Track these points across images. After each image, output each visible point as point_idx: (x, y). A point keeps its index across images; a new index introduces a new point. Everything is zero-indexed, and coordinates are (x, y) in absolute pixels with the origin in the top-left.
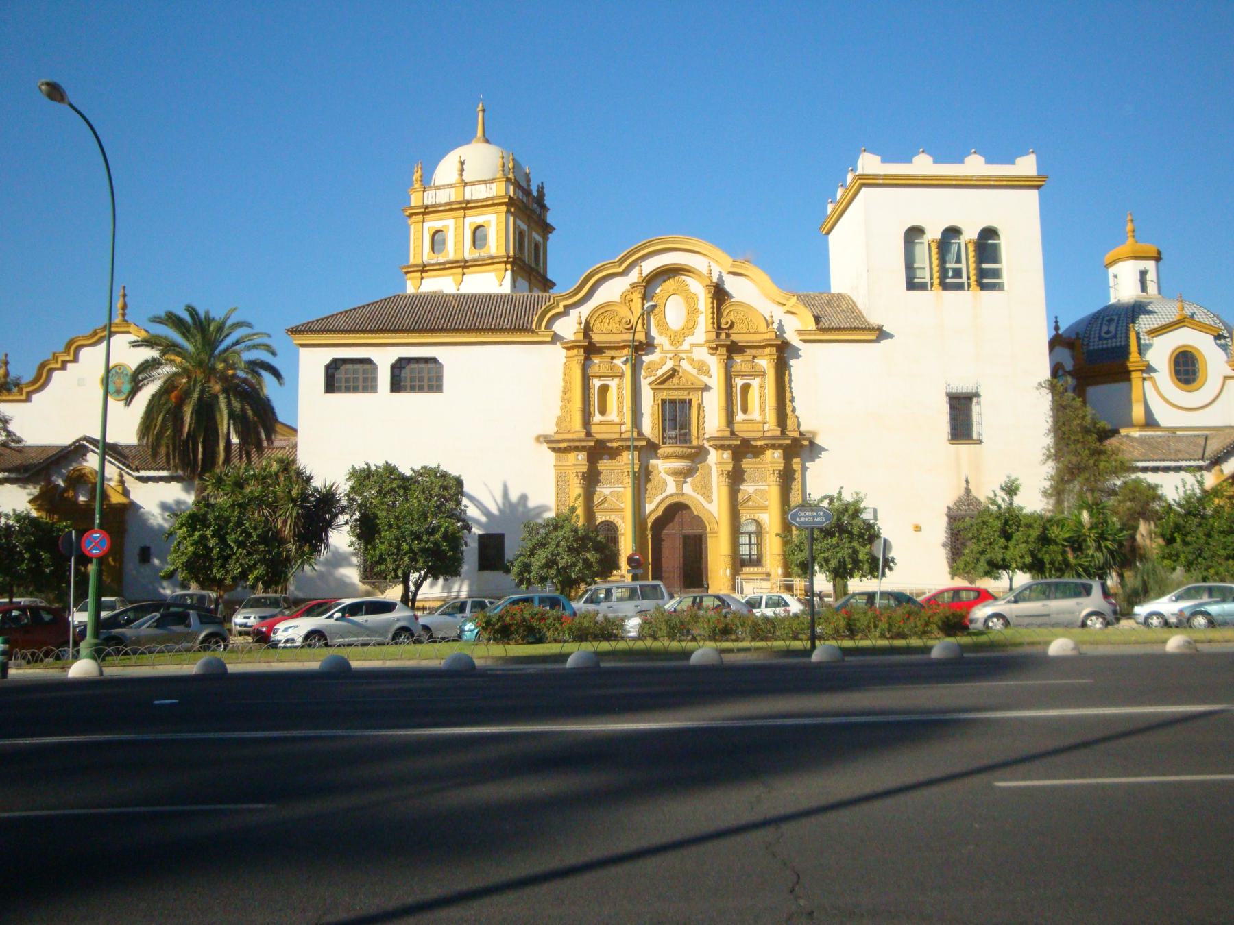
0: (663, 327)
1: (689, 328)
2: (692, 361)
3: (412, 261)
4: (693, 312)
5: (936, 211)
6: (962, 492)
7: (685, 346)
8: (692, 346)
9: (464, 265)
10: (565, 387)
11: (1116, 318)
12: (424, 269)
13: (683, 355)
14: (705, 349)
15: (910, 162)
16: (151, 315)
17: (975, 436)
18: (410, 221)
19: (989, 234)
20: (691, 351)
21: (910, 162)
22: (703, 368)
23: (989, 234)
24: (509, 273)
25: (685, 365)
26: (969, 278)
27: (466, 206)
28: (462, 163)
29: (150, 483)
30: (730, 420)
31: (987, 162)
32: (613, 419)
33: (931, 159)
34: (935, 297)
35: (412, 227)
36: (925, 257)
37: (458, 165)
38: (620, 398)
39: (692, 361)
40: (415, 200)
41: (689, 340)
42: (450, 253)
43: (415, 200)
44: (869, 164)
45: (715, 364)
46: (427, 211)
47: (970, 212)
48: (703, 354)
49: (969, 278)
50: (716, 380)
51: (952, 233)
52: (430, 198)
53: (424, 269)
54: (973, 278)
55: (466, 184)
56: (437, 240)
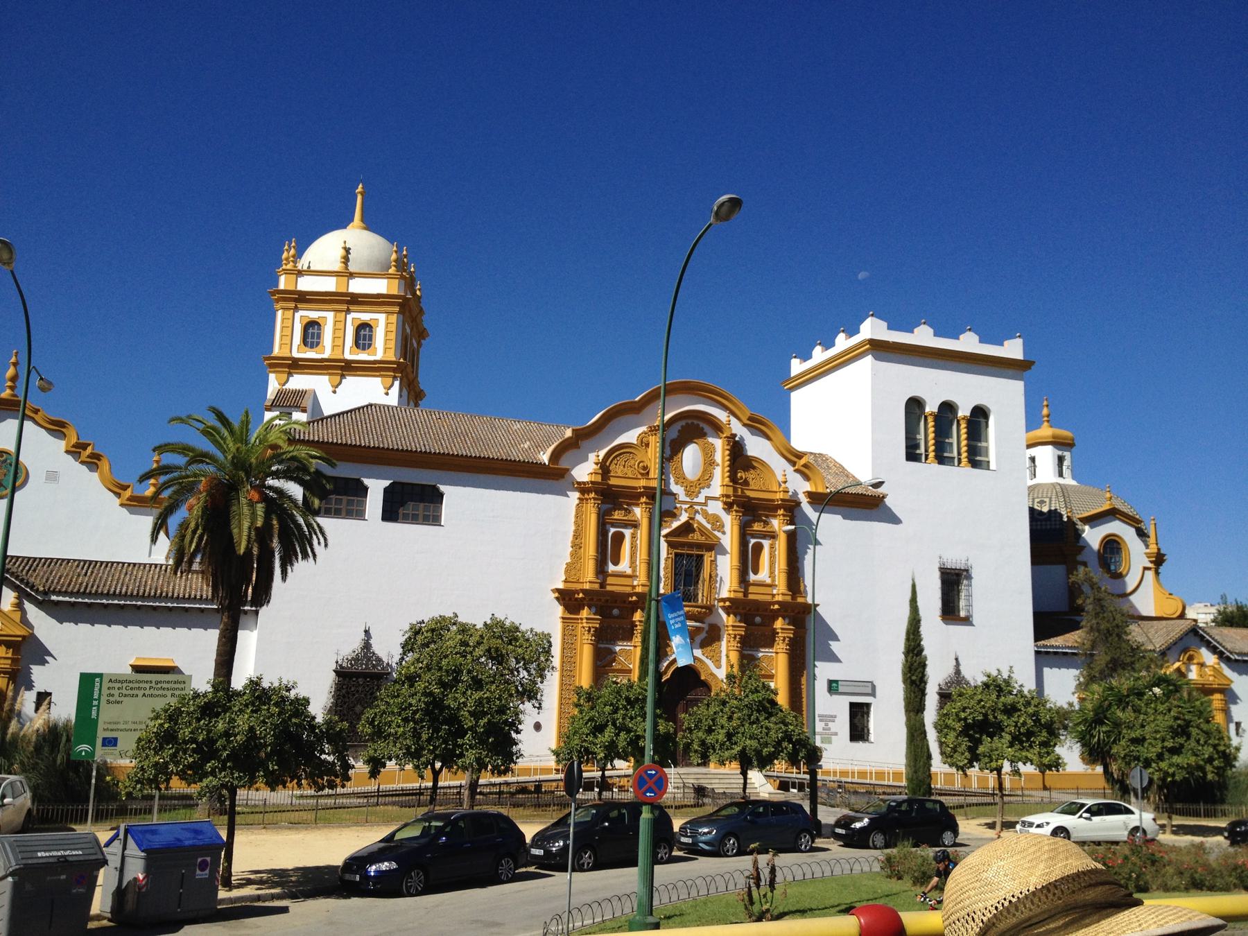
0: (681, 479)
1: (705, 480)
2: (706, 515)
3: (276, 351)
4: (710, 463)
5: (938, 386)
6: (951, 671)
7: (701, 499)
8: (707, 498)
9: (343, 368)
10: (575, 531)
11: (1047, 500)
12: (295, 366)
13: (698, 508)
14: (720, 505)
15: (912, 332)
16: (214, 405)
17: (963, 614)
18: (278, 306)
19: (912, 455)
20: (705, 504)
21: (912, 332)
22: (716, 522)
23: (980, 414)
24: (397, 383)
25: (699, 517)
26: (959, 454)
27: (356, 301)
28: (347, 250)
29: (919, 604)
30: (601, 570)
31: (981, 341)
32: (630, 567)
33: (976, 338)
34: (930, 469)
35: (280, 313)
36: (927, 435)
37: (342, 252)
38: (772, 556)
39: (706, 515)
40: (283, 283)
41: (705, 493)
42: (327, 350)
43: (283, 283)
44: (797, 367)
45: (730, 522)
46: (303, 298)
47: (966, 391)
48: (716, 508)
49: (959, 454)
50: (729, 538)
51: (948, 408)
52: (306, 284)
53: (295, 366)
54: (964, 455)
55: (352, 275)
56: (311, 332)
